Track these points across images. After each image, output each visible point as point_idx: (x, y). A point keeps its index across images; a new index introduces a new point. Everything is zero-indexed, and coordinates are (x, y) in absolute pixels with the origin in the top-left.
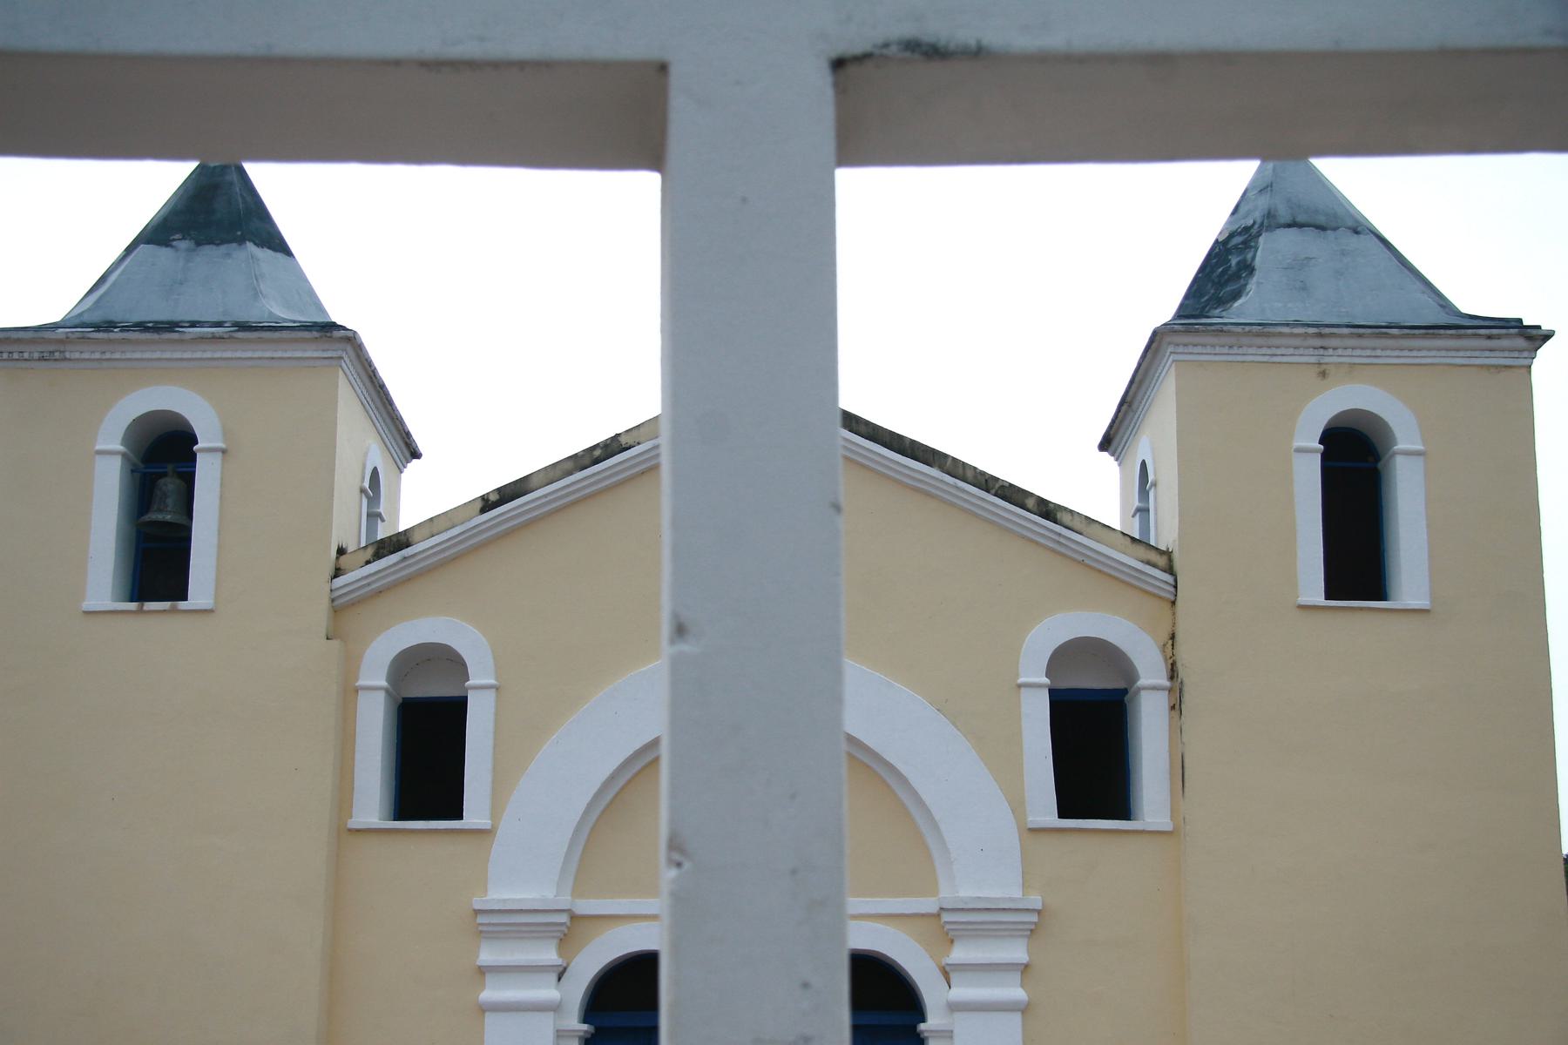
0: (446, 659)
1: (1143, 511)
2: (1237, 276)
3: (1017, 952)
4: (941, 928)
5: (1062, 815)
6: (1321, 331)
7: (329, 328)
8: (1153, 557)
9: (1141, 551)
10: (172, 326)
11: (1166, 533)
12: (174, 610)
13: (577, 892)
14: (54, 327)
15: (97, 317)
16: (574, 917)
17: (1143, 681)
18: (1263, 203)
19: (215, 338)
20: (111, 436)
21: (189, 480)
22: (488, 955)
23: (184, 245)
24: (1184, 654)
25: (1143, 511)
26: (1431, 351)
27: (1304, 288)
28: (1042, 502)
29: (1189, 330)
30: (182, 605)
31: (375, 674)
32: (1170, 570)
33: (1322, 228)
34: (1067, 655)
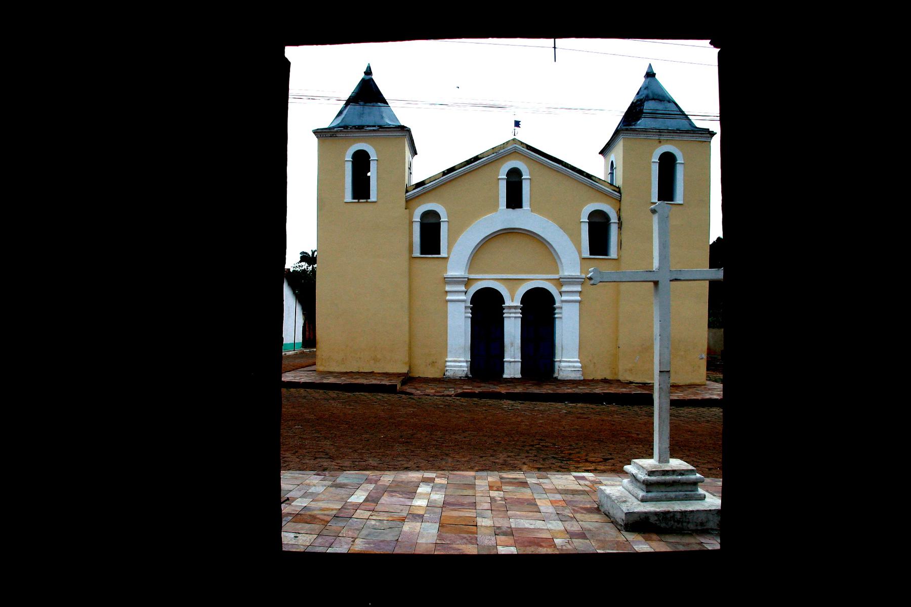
0: (434, 214)
1: (612, 174)
3: (579, 288)
4: (560, 282)
5: (422, 254)
11: (618, 182)
15: (343, 124)
17: (612, 221)
18: (646, 92)
20: (349, 157)
22: (448, 288)
24: (623, 215)
26: (686, 137)
32: (619, 192)
33: (661, 101)
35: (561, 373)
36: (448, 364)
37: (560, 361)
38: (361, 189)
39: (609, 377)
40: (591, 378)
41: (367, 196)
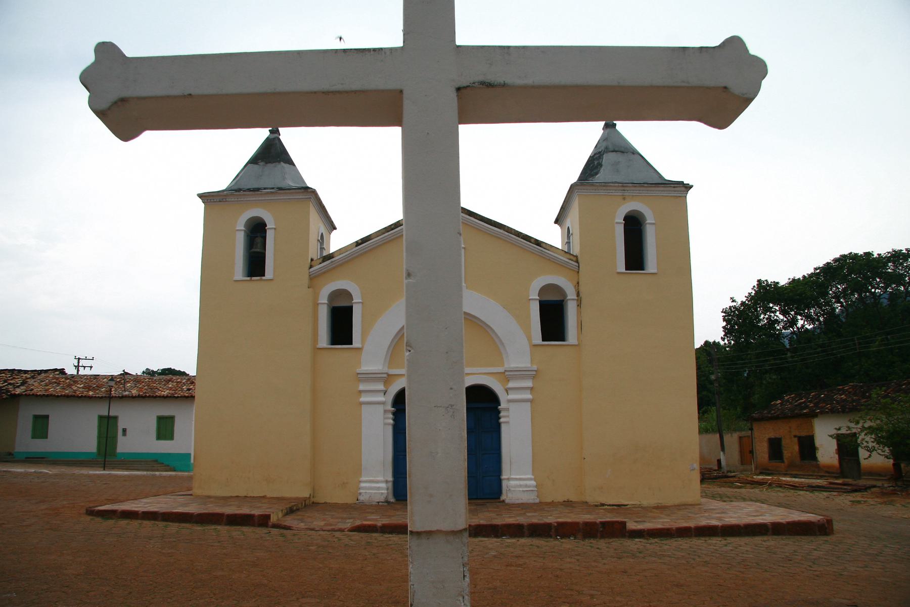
1: (568, 243)
2: (597, 167)
3: (529, 384)
4: (506, 376)
5: (543, 340)
6: (623, 185)
7: (307, 188)
8: (572, 257)
9: (568, 256)
10: (258, 190)
11: (576, 250)
12: (261, 280)
13: (389, 368)
14: (223, 191)
15: (236, 188)
16: (389, 375)
18: (604, 144)
19: (272, 193)
20: (241, 224)
21: (265, 238)
23: (262, 163)
25: (568, 243)
27: (618, 171)
28: (536, 240)
29: (582, 184)
30: (264, 278)
31: (324, 299)
32: (577, 262)
33: (623, 152)
34: (544, 290)
35: (510, 495)
36: (363, 485)
37: (508, 479)
38: (256, 265)
39: (573, 498)
40: (549, 500)
41: (262, 273)
